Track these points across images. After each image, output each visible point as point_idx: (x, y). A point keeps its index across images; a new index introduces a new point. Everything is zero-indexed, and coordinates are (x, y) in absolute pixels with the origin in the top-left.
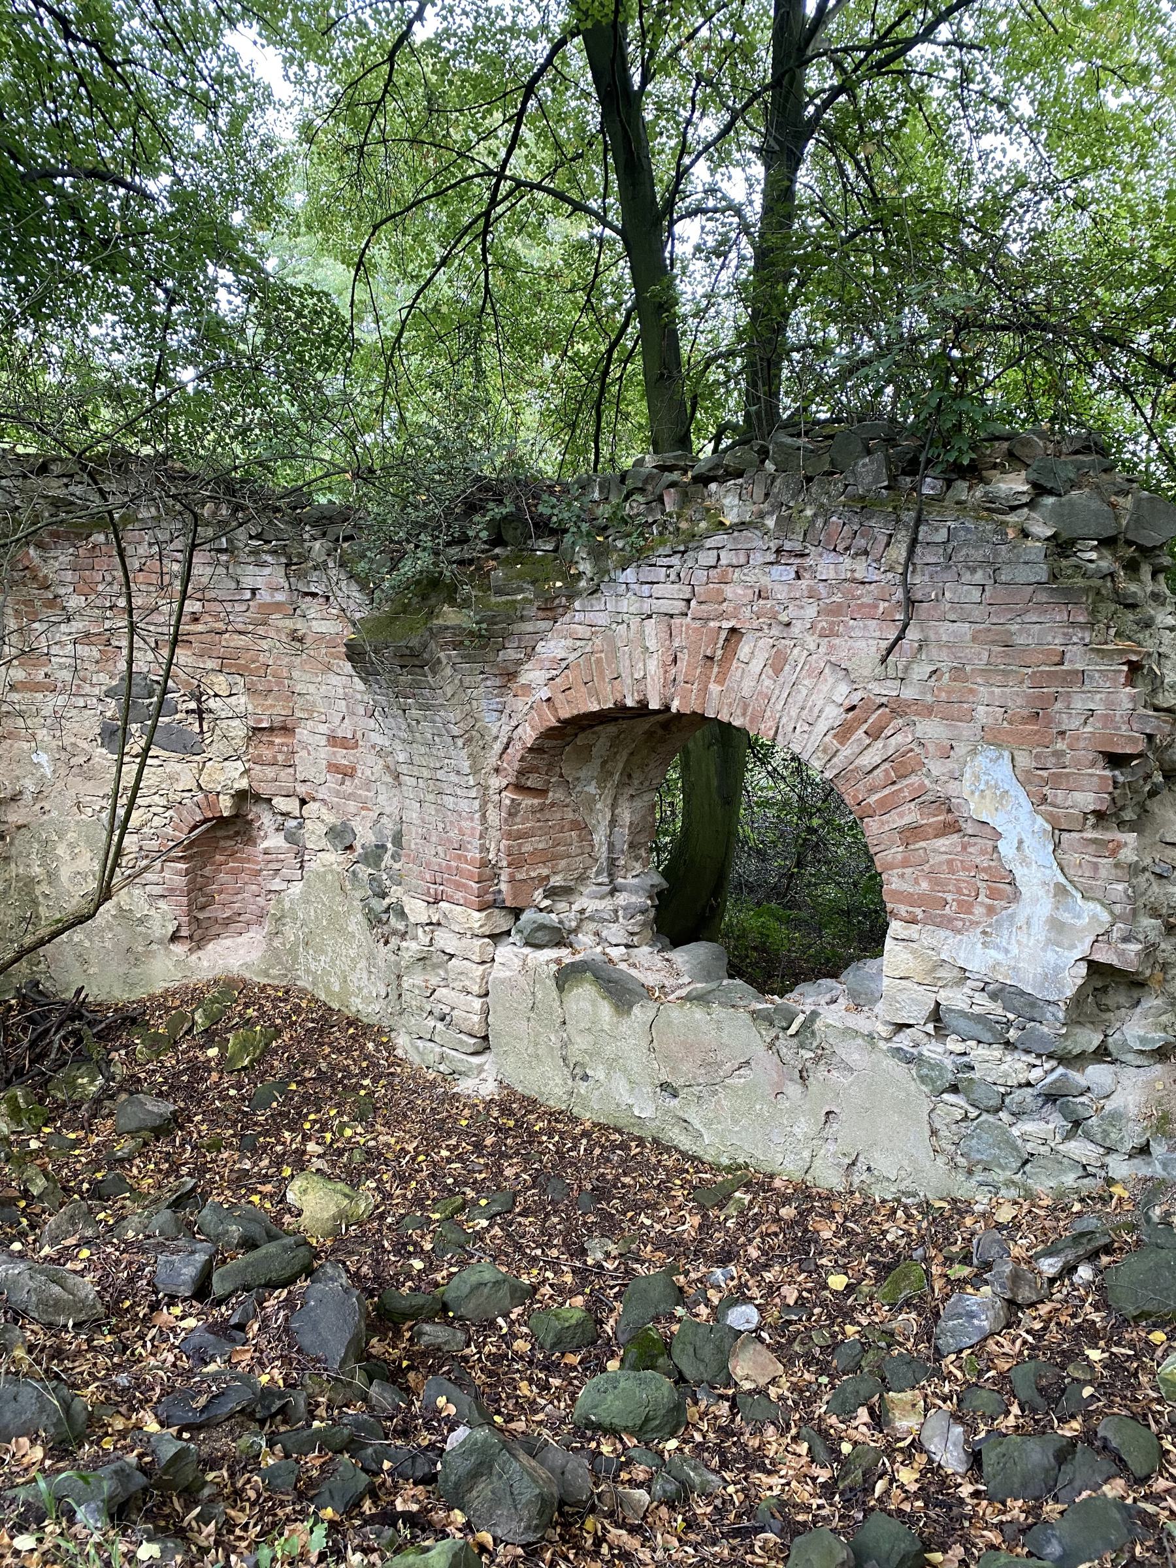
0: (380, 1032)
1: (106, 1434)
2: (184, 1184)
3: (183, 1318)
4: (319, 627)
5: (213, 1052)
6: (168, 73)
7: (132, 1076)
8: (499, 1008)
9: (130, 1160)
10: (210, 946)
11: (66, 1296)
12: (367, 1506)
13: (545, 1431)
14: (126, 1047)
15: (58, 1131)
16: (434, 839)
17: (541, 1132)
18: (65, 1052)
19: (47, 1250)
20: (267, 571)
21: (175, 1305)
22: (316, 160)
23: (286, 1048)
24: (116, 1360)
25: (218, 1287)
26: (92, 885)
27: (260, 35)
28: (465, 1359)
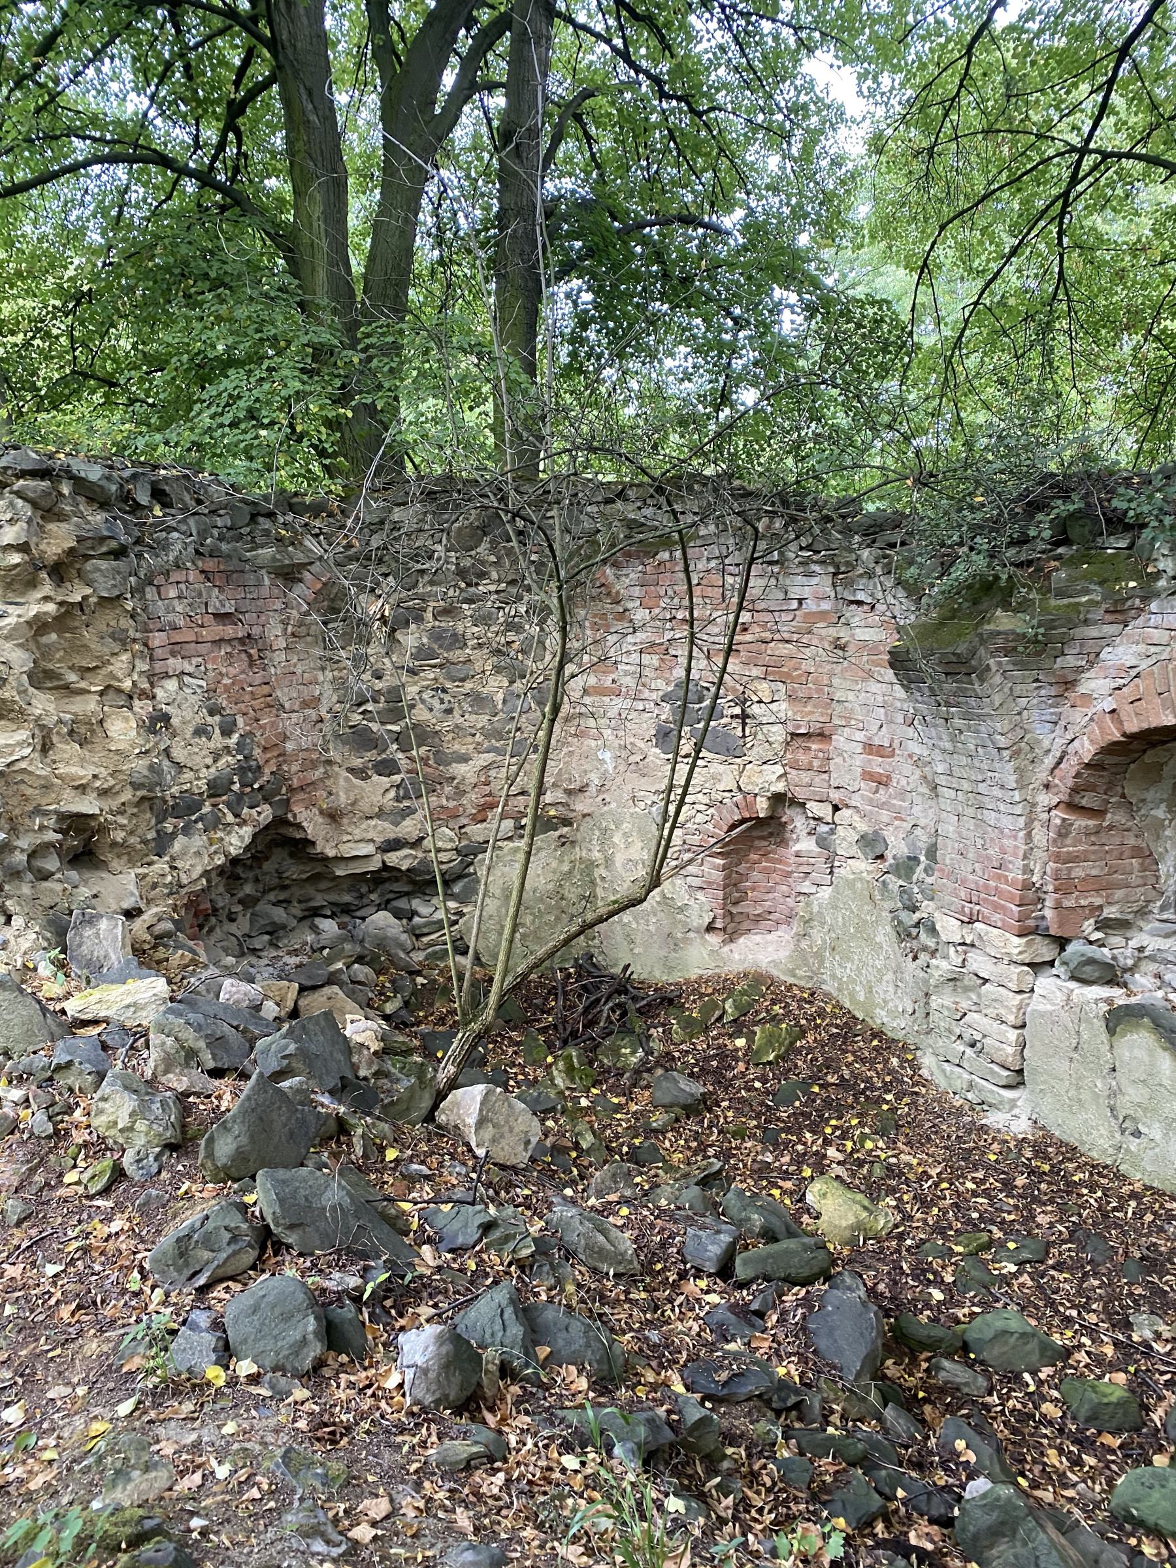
0: (905, 1048)
1: (639, 1383)
2: (711, 1164)
3: (707, 1292)
4: (863, 634)
5: (741, 1042)
6: (748, 112)
7: (668, 1054)
8: (1037, 1044)
9: (663, 1133)
10: (742, 940)
11: (609, 1247)
12: (879, 1528)
13: (1076, 1510)
14: (664, 1025)
15: (604, 1093)
16: (971, 855)
17: (1081, 1183)
18: (611, 1022)
19: (592, 1201)
20: (815, 581)
21: (701, 1278)
22: (884, 170)
23: (810, 1050)
24: (648, 1316)
25: (741, 1271)
26: (642, 872)
27: (836, 57)
28: (987, 1407)
